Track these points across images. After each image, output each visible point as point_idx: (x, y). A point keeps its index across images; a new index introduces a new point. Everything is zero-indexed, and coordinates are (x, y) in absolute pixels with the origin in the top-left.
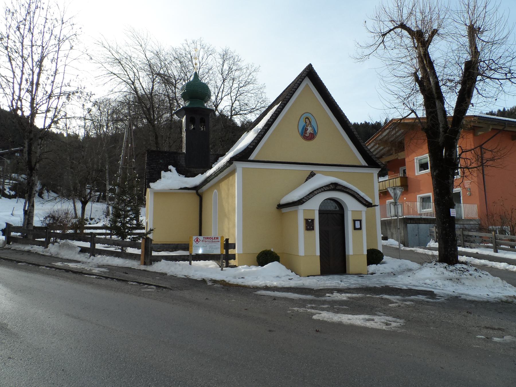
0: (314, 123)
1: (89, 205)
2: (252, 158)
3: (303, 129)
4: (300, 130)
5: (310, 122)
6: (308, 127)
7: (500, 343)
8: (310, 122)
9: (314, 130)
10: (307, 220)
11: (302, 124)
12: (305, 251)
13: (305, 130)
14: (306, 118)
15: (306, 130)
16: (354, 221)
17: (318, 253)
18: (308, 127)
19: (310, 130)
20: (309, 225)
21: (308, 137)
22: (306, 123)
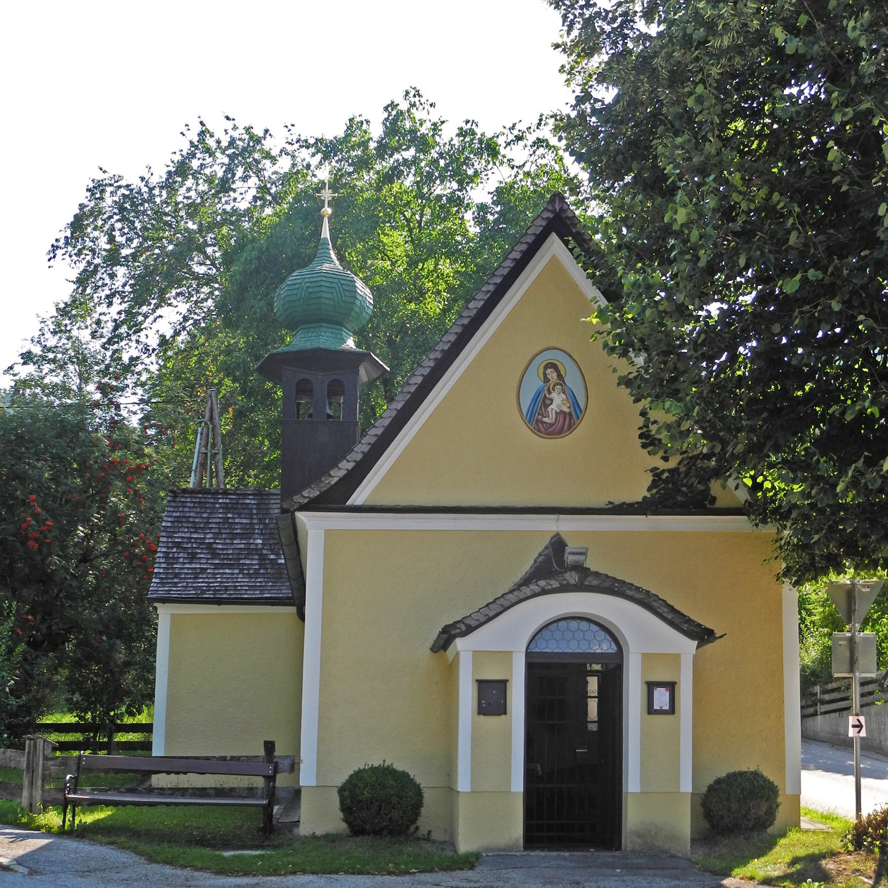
0: (572, 380)
1: (589, 694)
2: (359, 497)
3: (535, 400)
4: (526, 404)
5: (560, 376)
6: (554, 395)
7: (397, 150)
8: (560, 376)
9: (575, 403)
10: (483, 685)
11: (533, 383)
12: (473, 780)
13: (542, 401)
14: (546, 367)
15: (546, 403)
16: (651, 686)
17: (518, 785)
18: (554, 395)
19: (558, 402)
20: (491, 697)
21: (552, 425)
22: (546, 380)
